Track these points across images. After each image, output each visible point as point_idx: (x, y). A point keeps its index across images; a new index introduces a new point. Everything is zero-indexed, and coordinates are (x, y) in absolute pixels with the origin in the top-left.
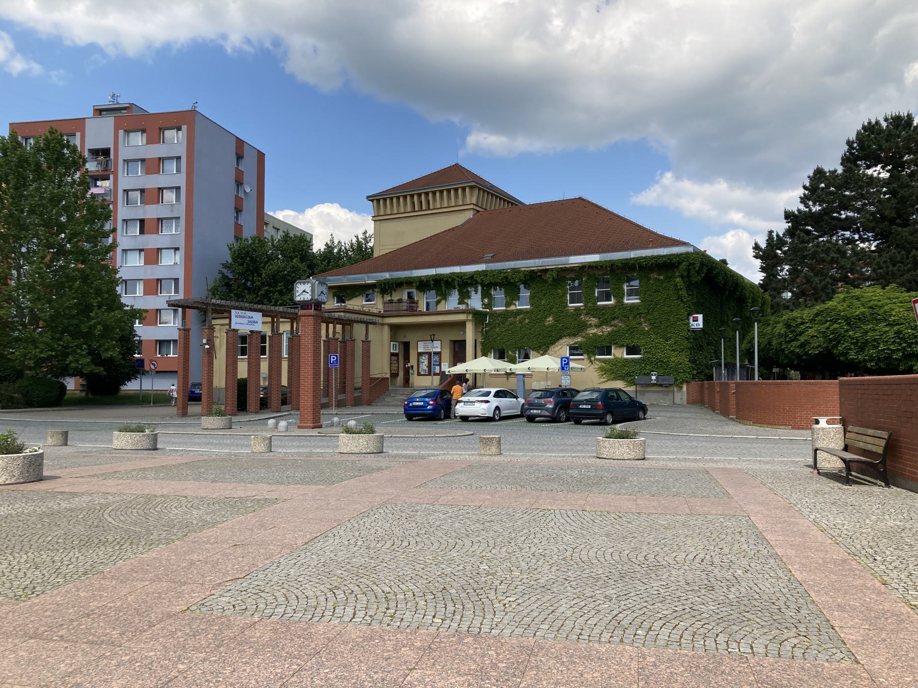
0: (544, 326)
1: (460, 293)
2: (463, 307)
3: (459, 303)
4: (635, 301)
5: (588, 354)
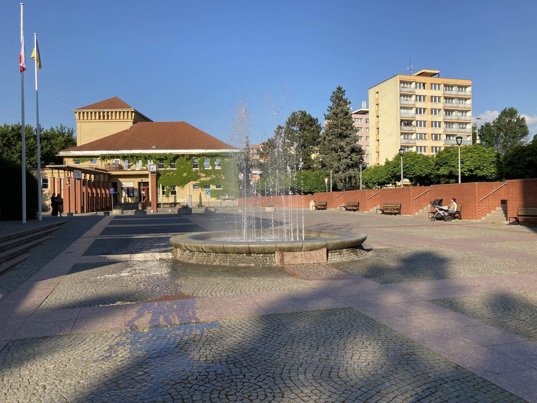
1: (143, 162)
3: (142, 166)
4: (220, 168)
5: (201, 188)
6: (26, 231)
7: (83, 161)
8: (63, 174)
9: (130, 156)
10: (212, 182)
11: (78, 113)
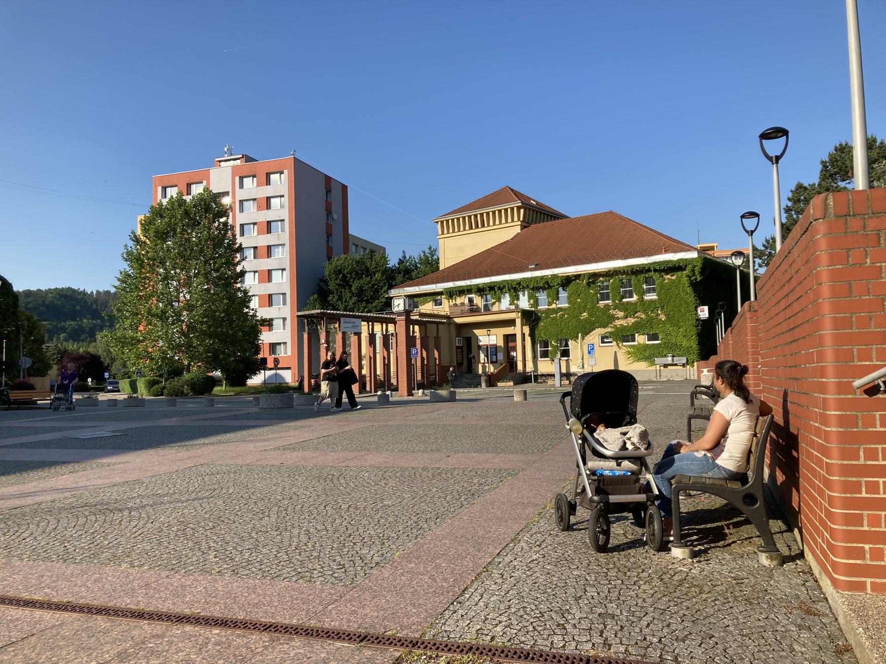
0: (580, 319)
1: (511, 296)
2: (513, 307)
3: (510, 304)
5: (617, 342)
6: (166, 424)
7: (424, 303)
8: (366, 327)
9: (489, 287)
10: (638, 327)
11: (439, 223)
